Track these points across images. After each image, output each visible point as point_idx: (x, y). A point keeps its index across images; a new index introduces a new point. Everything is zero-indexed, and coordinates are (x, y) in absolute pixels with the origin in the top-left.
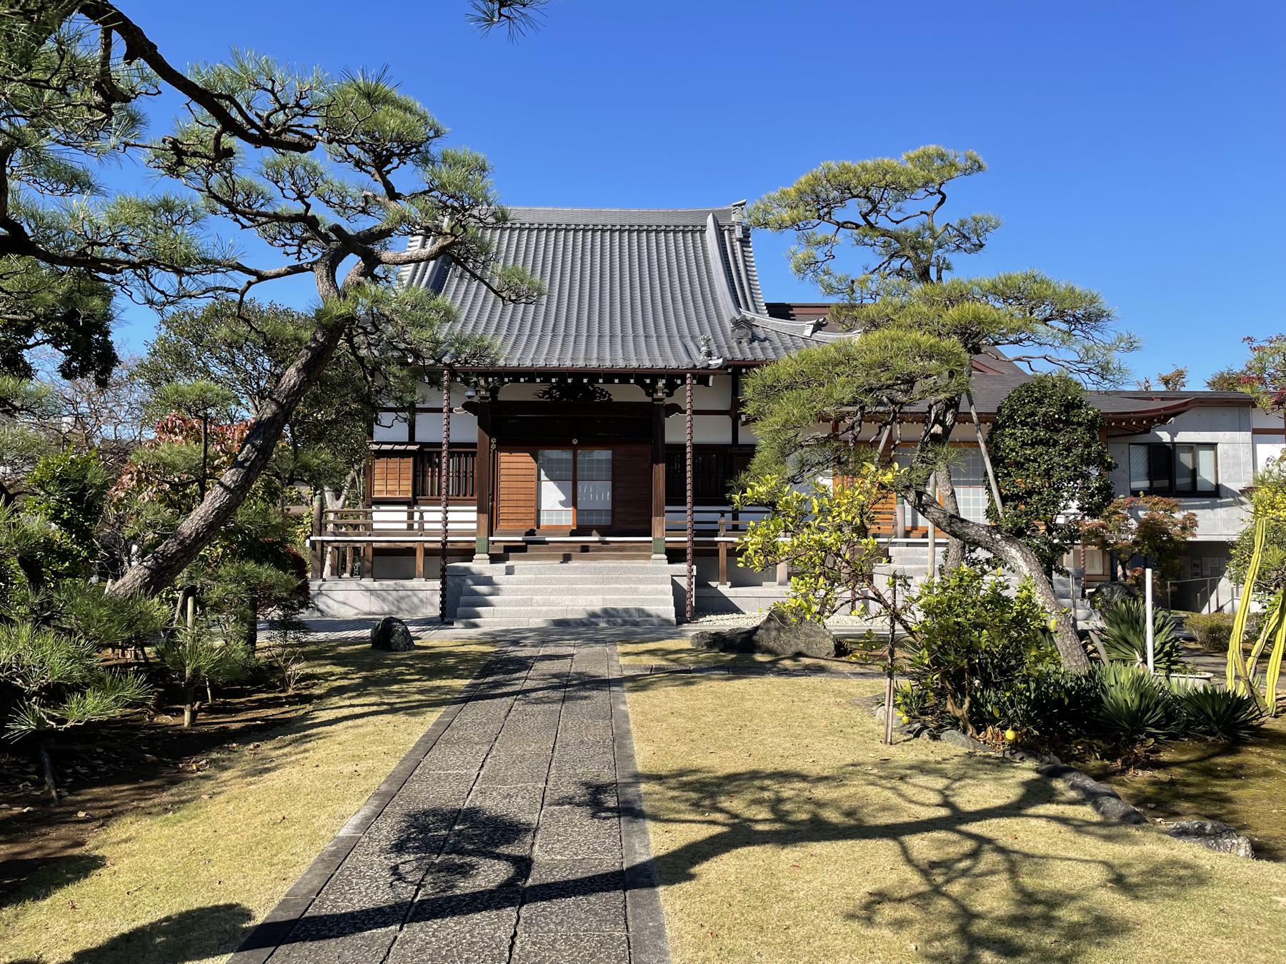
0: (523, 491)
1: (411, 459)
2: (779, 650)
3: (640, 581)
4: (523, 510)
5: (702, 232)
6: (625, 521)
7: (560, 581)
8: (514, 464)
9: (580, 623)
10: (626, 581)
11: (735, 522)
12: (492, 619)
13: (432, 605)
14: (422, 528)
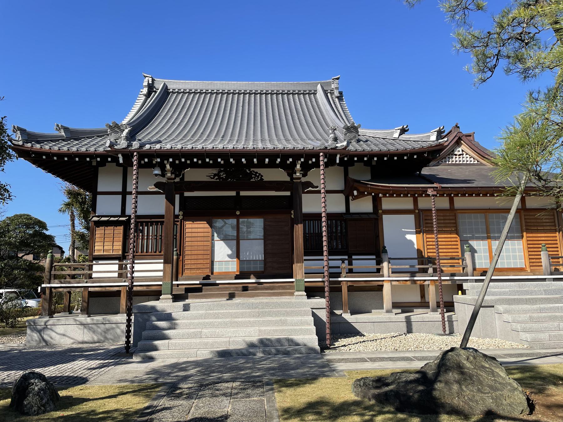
0: (201, 248)
1: (122, 227)
2: (466, 409)
3: (288, 314)
4: (201, 261)
5: (315, 94)
6: (275, 266)
7: (225, 316)
8: (195, 229)
10: (277, 314)
11: (350, 267)
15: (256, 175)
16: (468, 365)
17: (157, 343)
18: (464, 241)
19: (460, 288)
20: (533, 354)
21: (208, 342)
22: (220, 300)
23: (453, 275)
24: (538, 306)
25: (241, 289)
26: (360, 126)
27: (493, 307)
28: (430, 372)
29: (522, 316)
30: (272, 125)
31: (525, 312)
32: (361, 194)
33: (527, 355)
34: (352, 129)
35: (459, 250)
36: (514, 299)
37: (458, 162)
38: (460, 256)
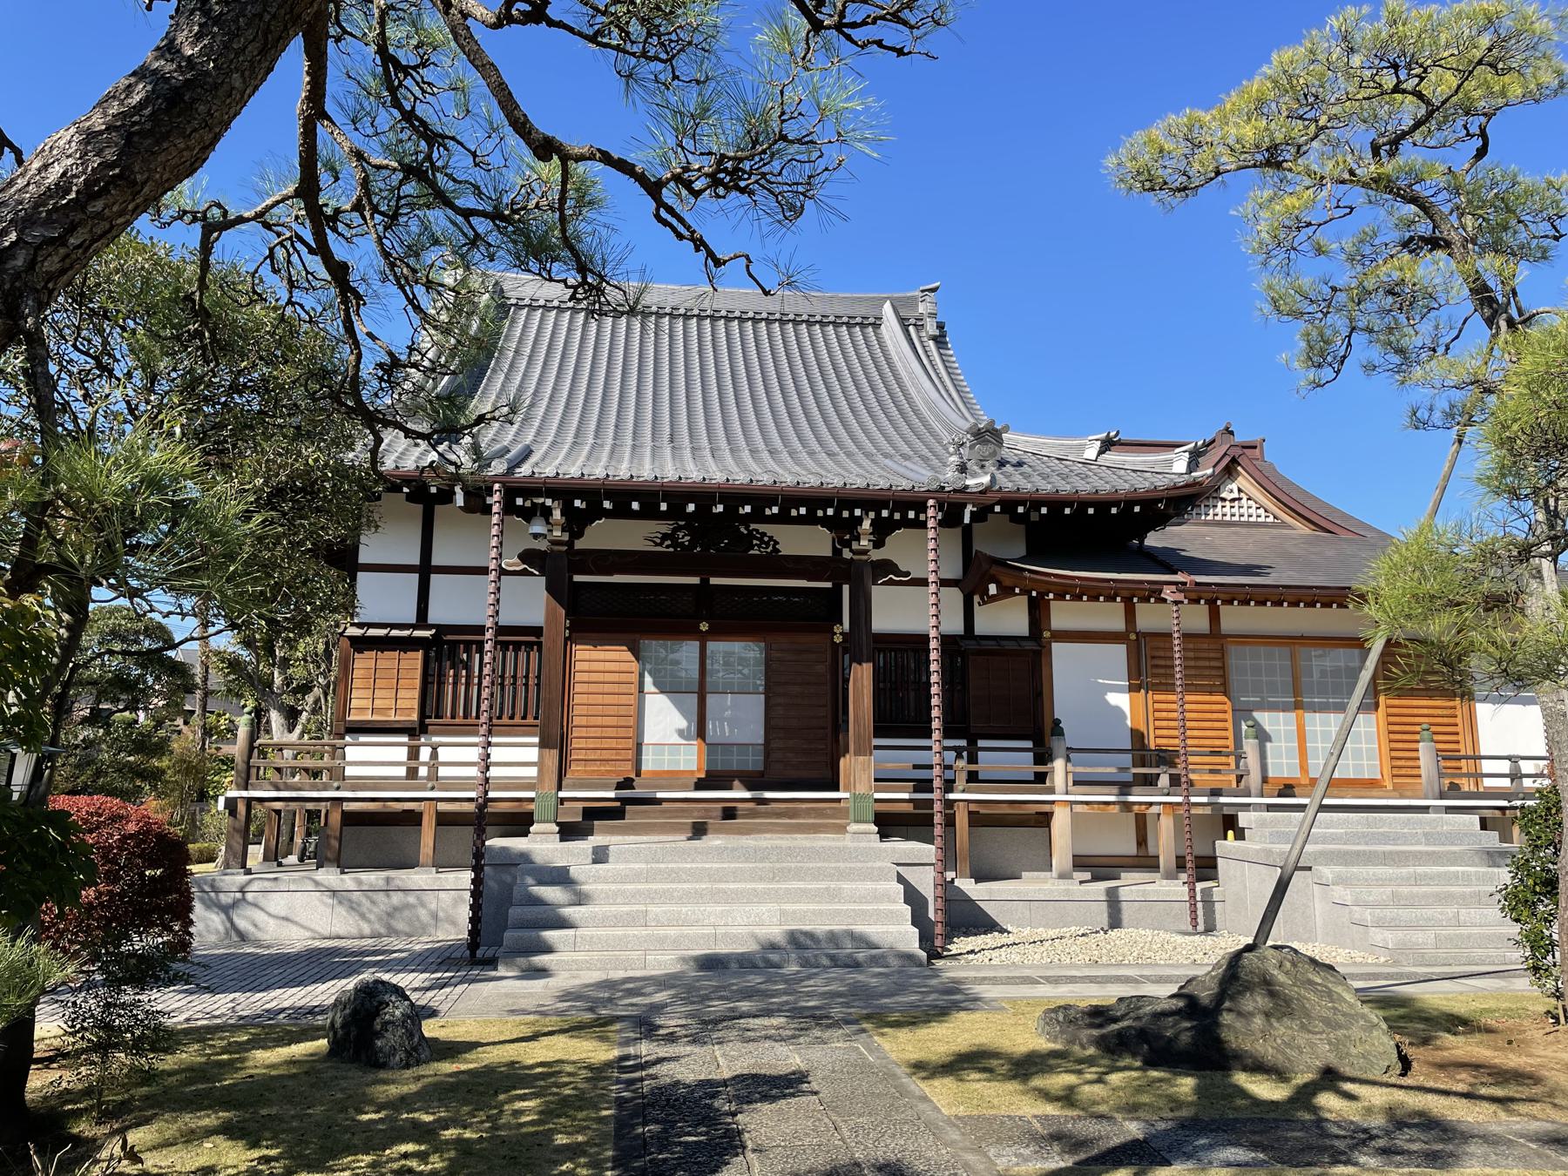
2: (1280, 1060)
3: (842, 875)
4: (613, 743)
5: (876, 326)
6: (793, 761)
8: (599, 665)
9: (745, 963)
10: (817, 875)
11: (973, 767)
12: (581, 956)
13: (454, 923)
14: (433, 775)
15: (761, 540)
16: (1281, 978)
17: (551, 935)
18: (1242, 712)
19: (1229, 823)
20: (1400, 975)
21: (666, 937)
22: (670, 838)
23: (1216, 792)
24: (1411, 869)
25: (719, 813)
26: (1006, 429)
27: (1310, 869)
28: (1205, 995)
29: (1376, 890)
30: (783, 409)
31: (1382, 882)
32: (1006, 592)
33: (1387, 976)
34: (988, 436)
35: (1230, 734)
36: (1358, 853)
37: (1228, 518)
38: (1232, 748)
